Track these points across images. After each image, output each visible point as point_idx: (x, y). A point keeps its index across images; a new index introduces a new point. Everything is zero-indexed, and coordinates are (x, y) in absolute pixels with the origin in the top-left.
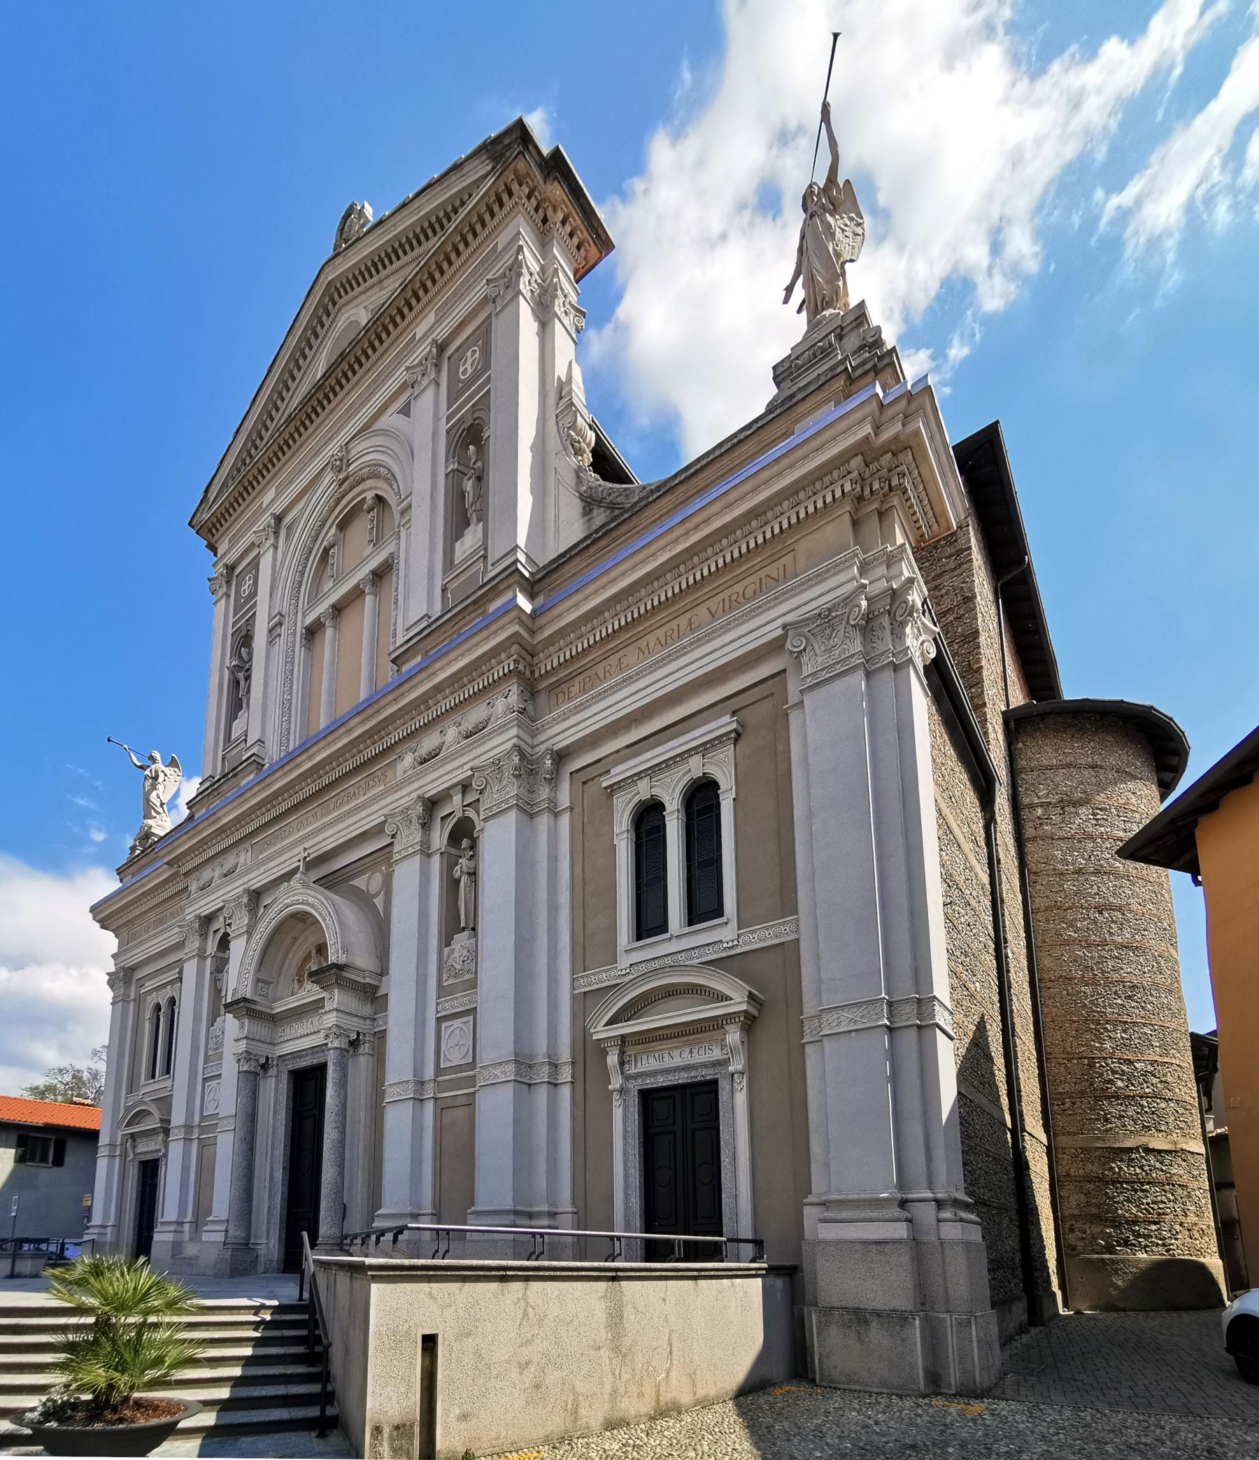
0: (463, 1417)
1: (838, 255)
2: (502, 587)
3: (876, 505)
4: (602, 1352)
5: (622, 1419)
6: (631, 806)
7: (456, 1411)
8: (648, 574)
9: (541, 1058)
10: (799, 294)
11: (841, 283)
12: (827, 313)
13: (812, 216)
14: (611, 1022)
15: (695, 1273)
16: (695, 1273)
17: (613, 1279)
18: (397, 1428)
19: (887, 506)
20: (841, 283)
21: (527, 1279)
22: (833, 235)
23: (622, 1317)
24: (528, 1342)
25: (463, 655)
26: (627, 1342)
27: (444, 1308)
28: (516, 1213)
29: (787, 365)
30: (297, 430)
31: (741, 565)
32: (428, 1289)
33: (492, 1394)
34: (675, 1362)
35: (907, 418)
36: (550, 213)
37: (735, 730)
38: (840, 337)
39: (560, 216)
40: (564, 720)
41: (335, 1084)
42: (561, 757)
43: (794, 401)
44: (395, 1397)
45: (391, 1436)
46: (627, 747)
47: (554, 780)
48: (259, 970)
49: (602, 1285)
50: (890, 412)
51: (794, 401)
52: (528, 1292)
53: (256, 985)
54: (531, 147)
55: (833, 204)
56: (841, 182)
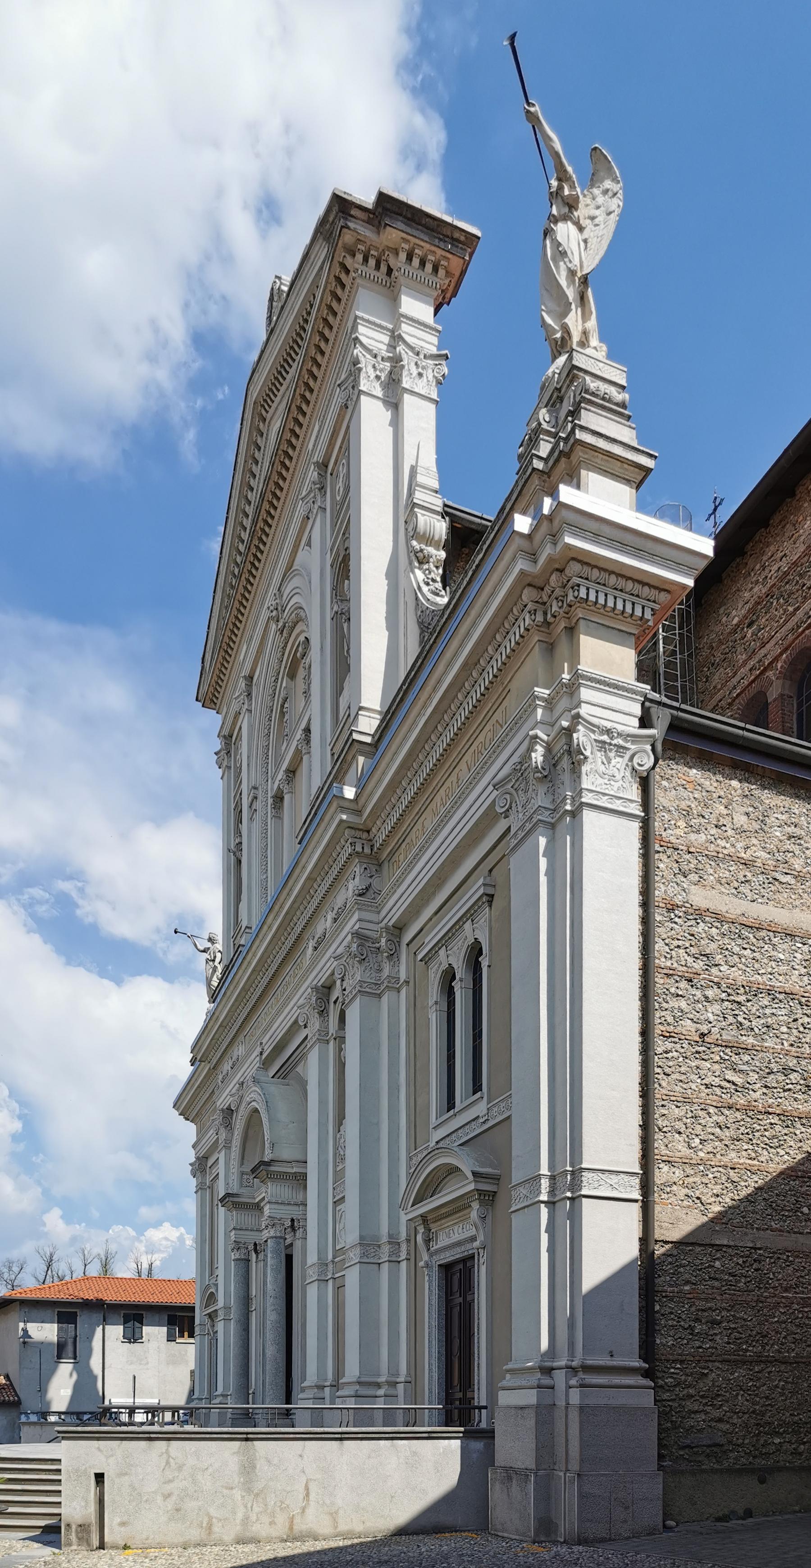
0: (123, 1524)
2: (349, 757)
3: (563, 625)
4: (234, 1491)
5: (252, 1538)
6: (439, 975)
7: (118, 1520)
8: (417, 741)
9: (385, 1239)
14: (412, 1206)
15: (339, 1436)
16: (339, 1436)
17: (247, 1439)
18: (80, 1526)
19: (574, 621)
21: (169, 1439)
23: (254, 1467)
24: (170, 1481)
25: (315, 847)
26: (258, 1486)
27: (107, 1457)
28: (359, 1383)
30: (248, 581)
31: (479, 712)
32: (97, 1446)
33: (143, 1512)
34: (312, 1503)
35: (555, 537)
36: (392, 262)
37: (485, 894)
39: (403, 256)
40: (393, 894)
41: (272, 1269)
42: (399, 929)
44: (78, 1508)
45: (76, 1531)
46: (436, 913)
47: (393, 956)
48: (242, 1164)
49: (237, 1444)
50: (538, 538)
52: (170, 1449)
53: (242, 1178)
54: (353, 212)
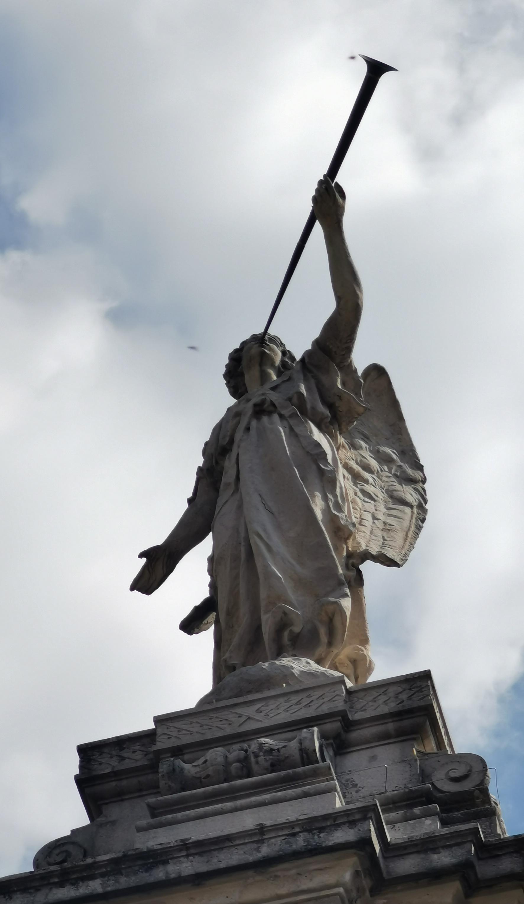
1: (342, 533)
10: (191, 580)
11: (347, 603)
12: (300, 665)
13: (261, 410)
20: (347, 603)
22: (328, 481)
29: (136, 758)
38: (339, 746)
43: (159, 874)
51: (159, 874)
55: (331, 406)
56: (361, 359)
